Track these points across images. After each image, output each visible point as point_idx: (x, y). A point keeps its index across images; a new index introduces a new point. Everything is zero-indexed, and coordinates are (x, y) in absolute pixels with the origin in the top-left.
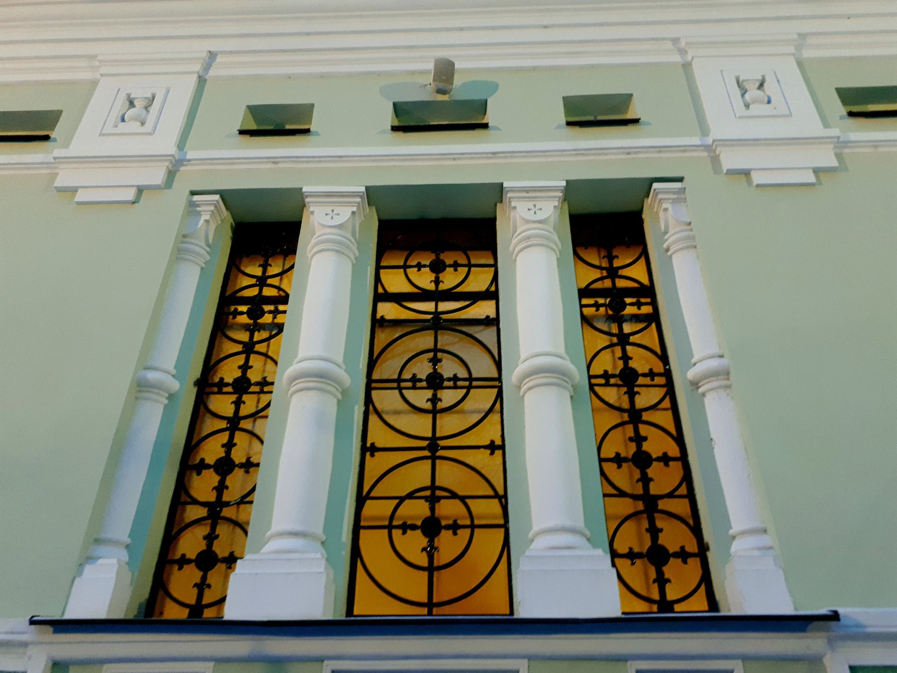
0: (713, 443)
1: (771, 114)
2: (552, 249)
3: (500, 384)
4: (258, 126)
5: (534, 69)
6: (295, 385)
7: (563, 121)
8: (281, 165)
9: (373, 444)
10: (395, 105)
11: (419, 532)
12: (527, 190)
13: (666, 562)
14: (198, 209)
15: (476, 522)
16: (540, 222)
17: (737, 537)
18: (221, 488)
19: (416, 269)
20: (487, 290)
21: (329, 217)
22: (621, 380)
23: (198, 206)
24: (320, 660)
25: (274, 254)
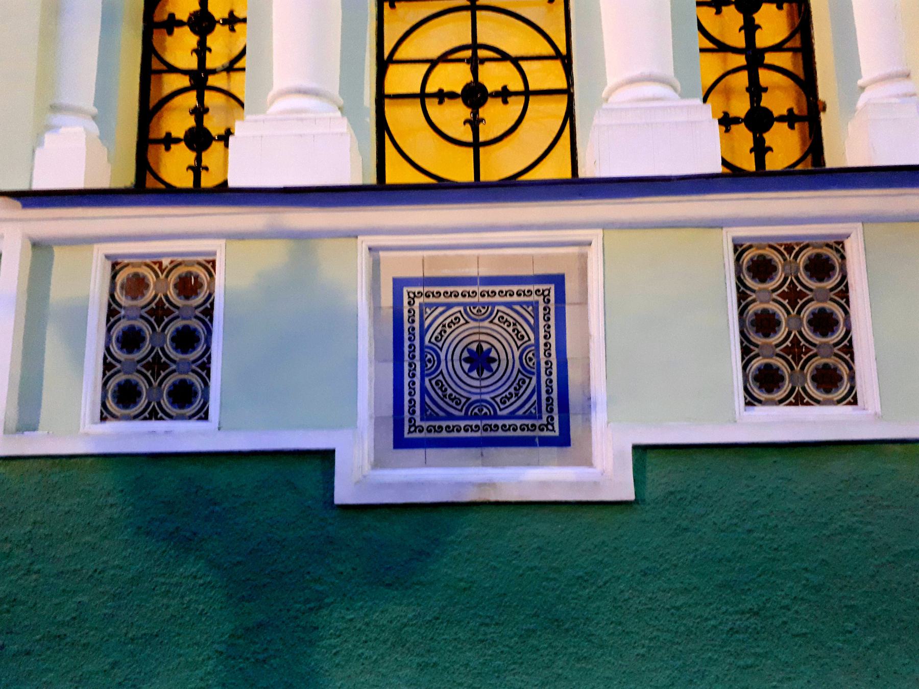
13: (768, 128)
17: (867, 89)
18: (202, 50)
24: (353, 235)
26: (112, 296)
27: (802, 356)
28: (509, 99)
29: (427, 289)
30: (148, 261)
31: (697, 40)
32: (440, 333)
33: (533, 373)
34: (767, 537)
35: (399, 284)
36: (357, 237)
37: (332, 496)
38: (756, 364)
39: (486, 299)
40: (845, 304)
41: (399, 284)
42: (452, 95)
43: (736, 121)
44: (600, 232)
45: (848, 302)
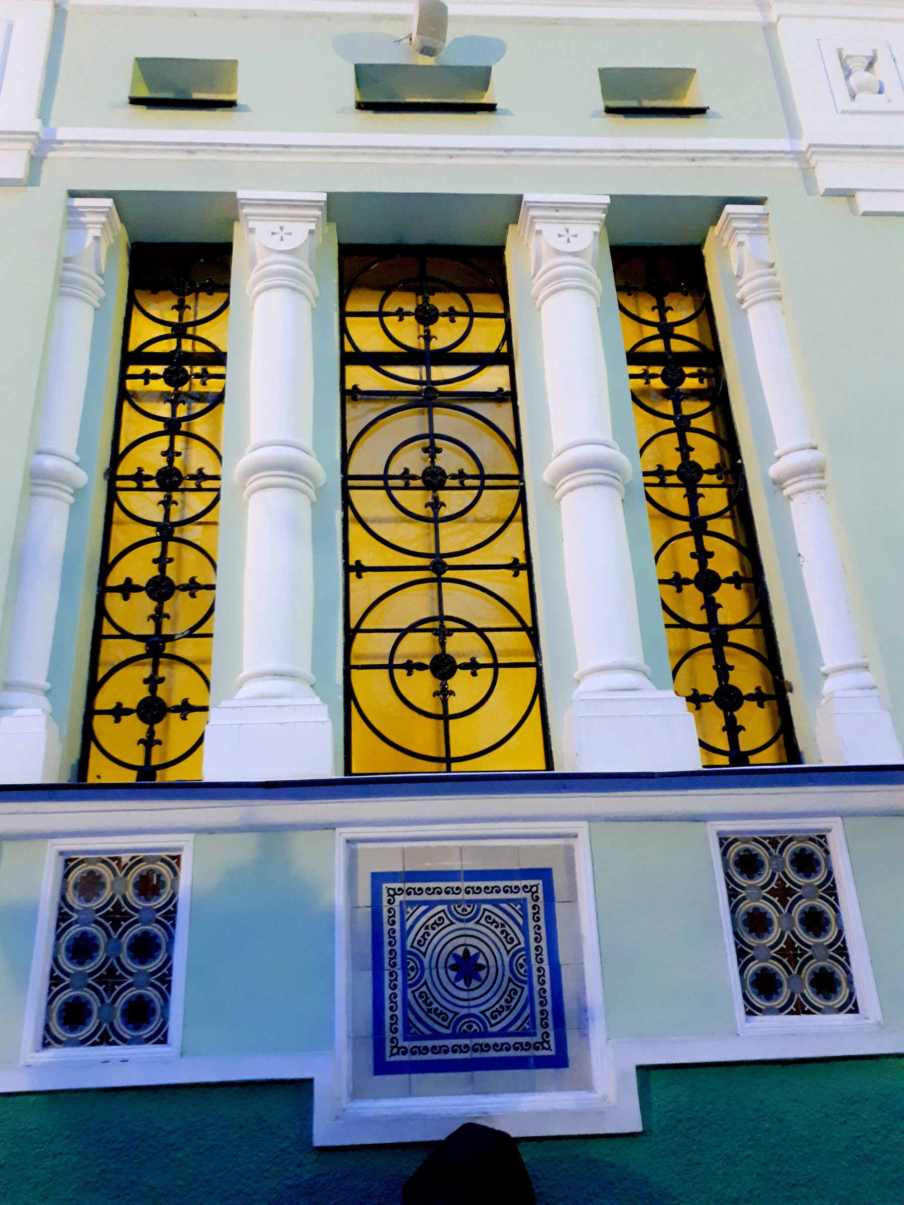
0: (801, 560)
1: (885, 109)
2: (592, 294)
3: (522, 484)
4: (150, 91)
5: (555, 22)
6: (255, 480)
7: (601, 106)
8: (199, 156)
9: (358, 562)
10: (358, 68)
11: (428, 672)
12: (556, 207)
14: (82, 219)
15: (500, 661)
16: (575, 254)
17: (829, 676)
19: (397, 318)
20: (498, 350)
21: (277, 237)
22: (680, 478)
23: (82, 214)
24: (330, 827)
25: (196, 290)
26: (63, 898)
27: (798, 958)
28: (478, 671)
29: (408, 885)
30: (105, 857)
31: (662, 618)
33: (524, 982)
34: (784, 1171)
35: (378, 879)
36: (334, 829)
37: (310, 1136)
38: (753, 967)
39: (471, 897)
40: (834, 902)
41: (378, 879)
42: (421, 667)
43: (706, 698)
44: (585, 824)
45: (836, 900)
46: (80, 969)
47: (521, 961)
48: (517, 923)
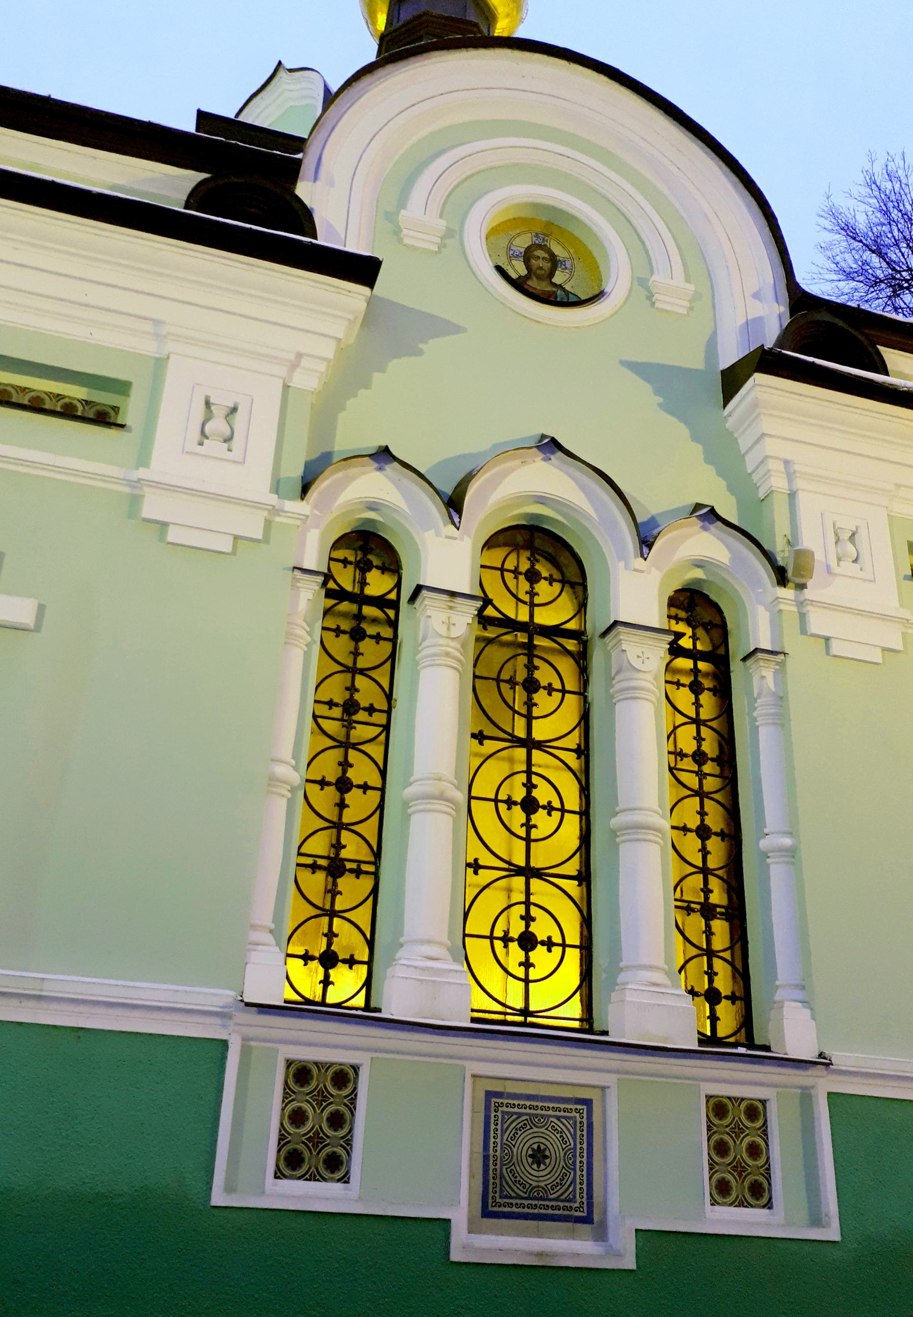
32: (514, 1135)
46: (297, 1131)
47: (570, 1156)
48: (570, 1132)
